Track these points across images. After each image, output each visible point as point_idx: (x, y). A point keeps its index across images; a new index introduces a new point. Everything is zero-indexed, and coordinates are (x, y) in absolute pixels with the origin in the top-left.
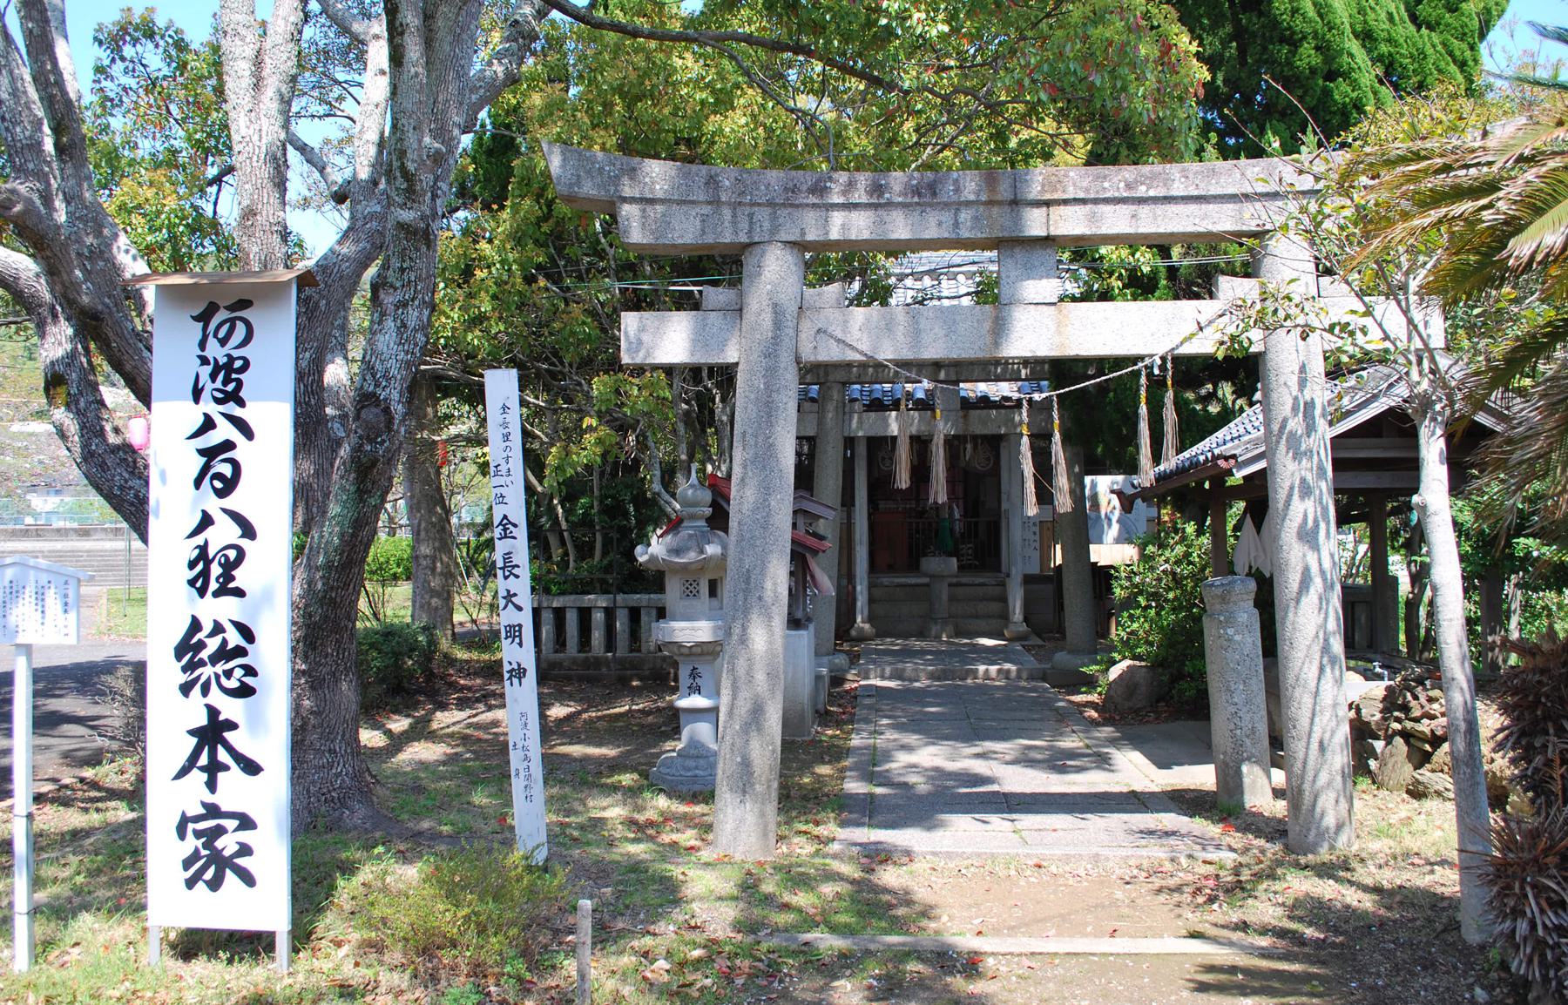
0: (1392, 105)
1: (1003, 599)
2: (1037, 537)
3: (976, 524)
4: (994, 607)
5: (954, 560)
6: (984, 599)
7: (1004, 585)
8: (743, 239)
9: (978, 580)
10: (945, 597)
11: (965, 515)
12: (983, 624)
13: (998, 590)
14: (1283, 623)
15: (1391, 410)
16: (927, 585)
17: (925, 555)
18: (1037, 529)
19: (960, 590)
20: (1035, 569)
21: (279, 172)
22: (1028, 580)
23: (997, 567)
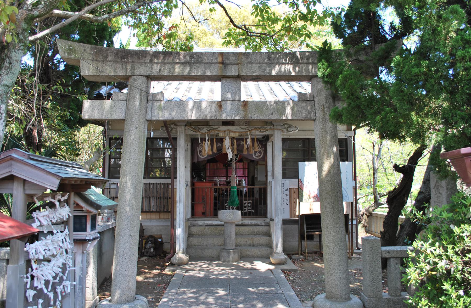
0: (53, 259)
1: (269, 235)
2: (288, 197)
3: (253, 189)
4: (264, 240)
5: (240, 212)
6: (258, 234)
7: (268, 225)
8: (130, 74)
9: (254, 222)
10: (233, 235)
11: (248, 184)
12: (256, 251)
13: (265, 228)
14: (186, 199)
15: (414, 152)
16: (223, 225)
17: (224, 208)
18: (288, 193)
19: (243, 229)
20: (287, 217)
21: (332, 298)
22: (285, 222)
23: (264, 214)
